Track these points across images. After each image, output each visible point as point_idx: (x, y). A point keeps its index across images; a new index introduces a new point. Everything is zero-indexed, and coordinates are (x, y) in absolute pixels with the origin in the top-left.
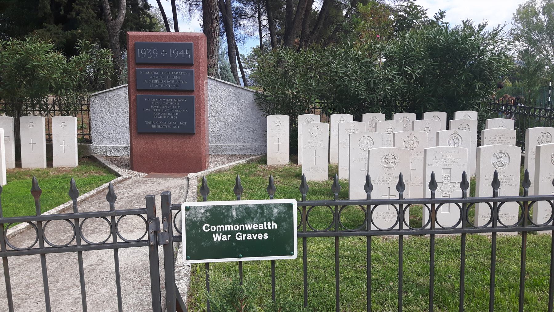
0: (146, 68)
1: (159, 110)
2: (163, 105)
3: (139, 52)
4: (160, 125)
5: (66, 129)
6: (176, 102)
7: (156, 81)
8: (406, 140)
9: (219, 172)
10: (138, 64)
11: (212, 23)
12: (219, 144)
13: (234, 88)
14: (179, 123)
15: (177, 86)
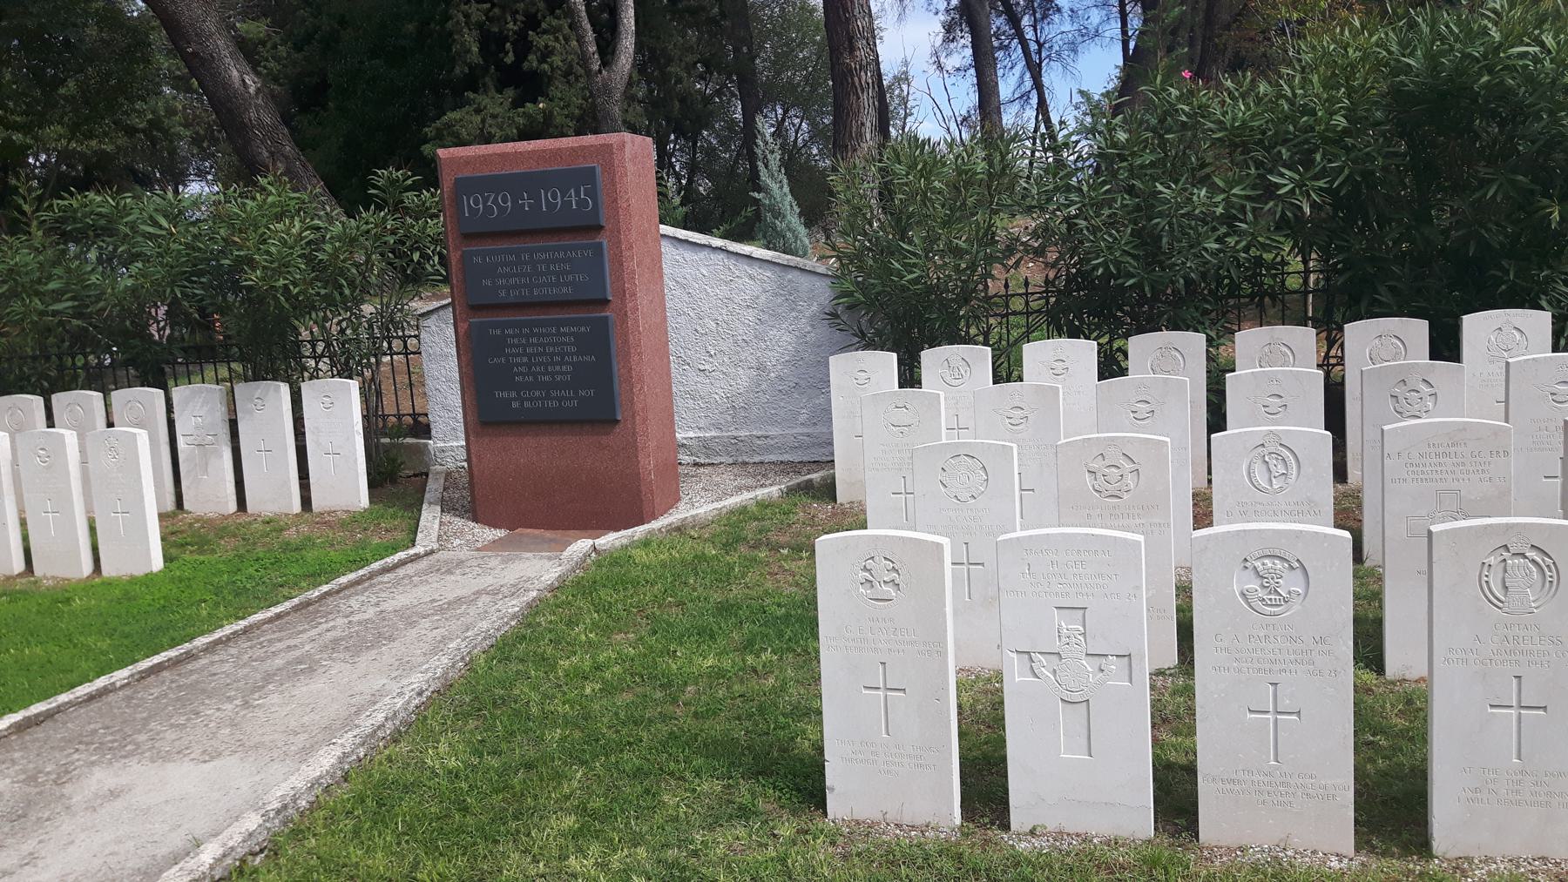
0: (490, 246)
1: (525, 360)
2: (533, 345)
3: (468, 202)
4: (531, 400)
5: (338, 409)
6: (565, 334)
7: (512, 281)
8: (1094, 466)
9: (678, 529)
10: (468, 237)
11: (852, 49)
12: (743, 433)
13: (777, 269)
14: (576, 393)
15: (564, 290)
